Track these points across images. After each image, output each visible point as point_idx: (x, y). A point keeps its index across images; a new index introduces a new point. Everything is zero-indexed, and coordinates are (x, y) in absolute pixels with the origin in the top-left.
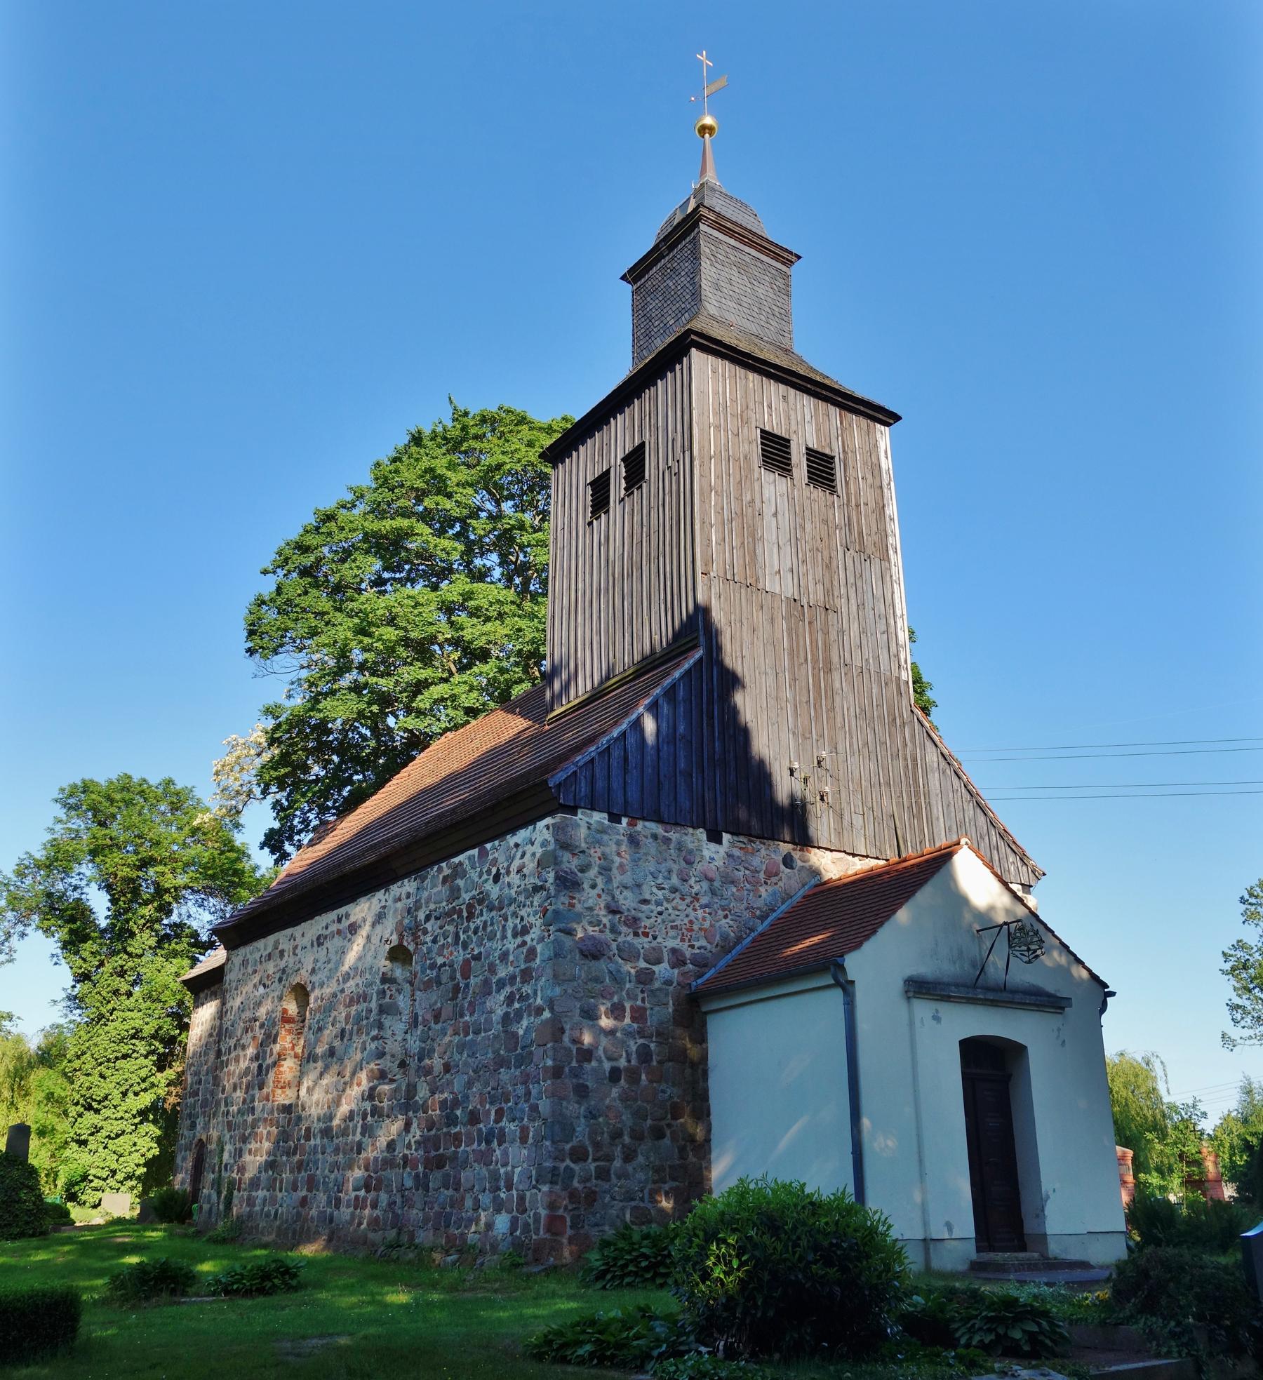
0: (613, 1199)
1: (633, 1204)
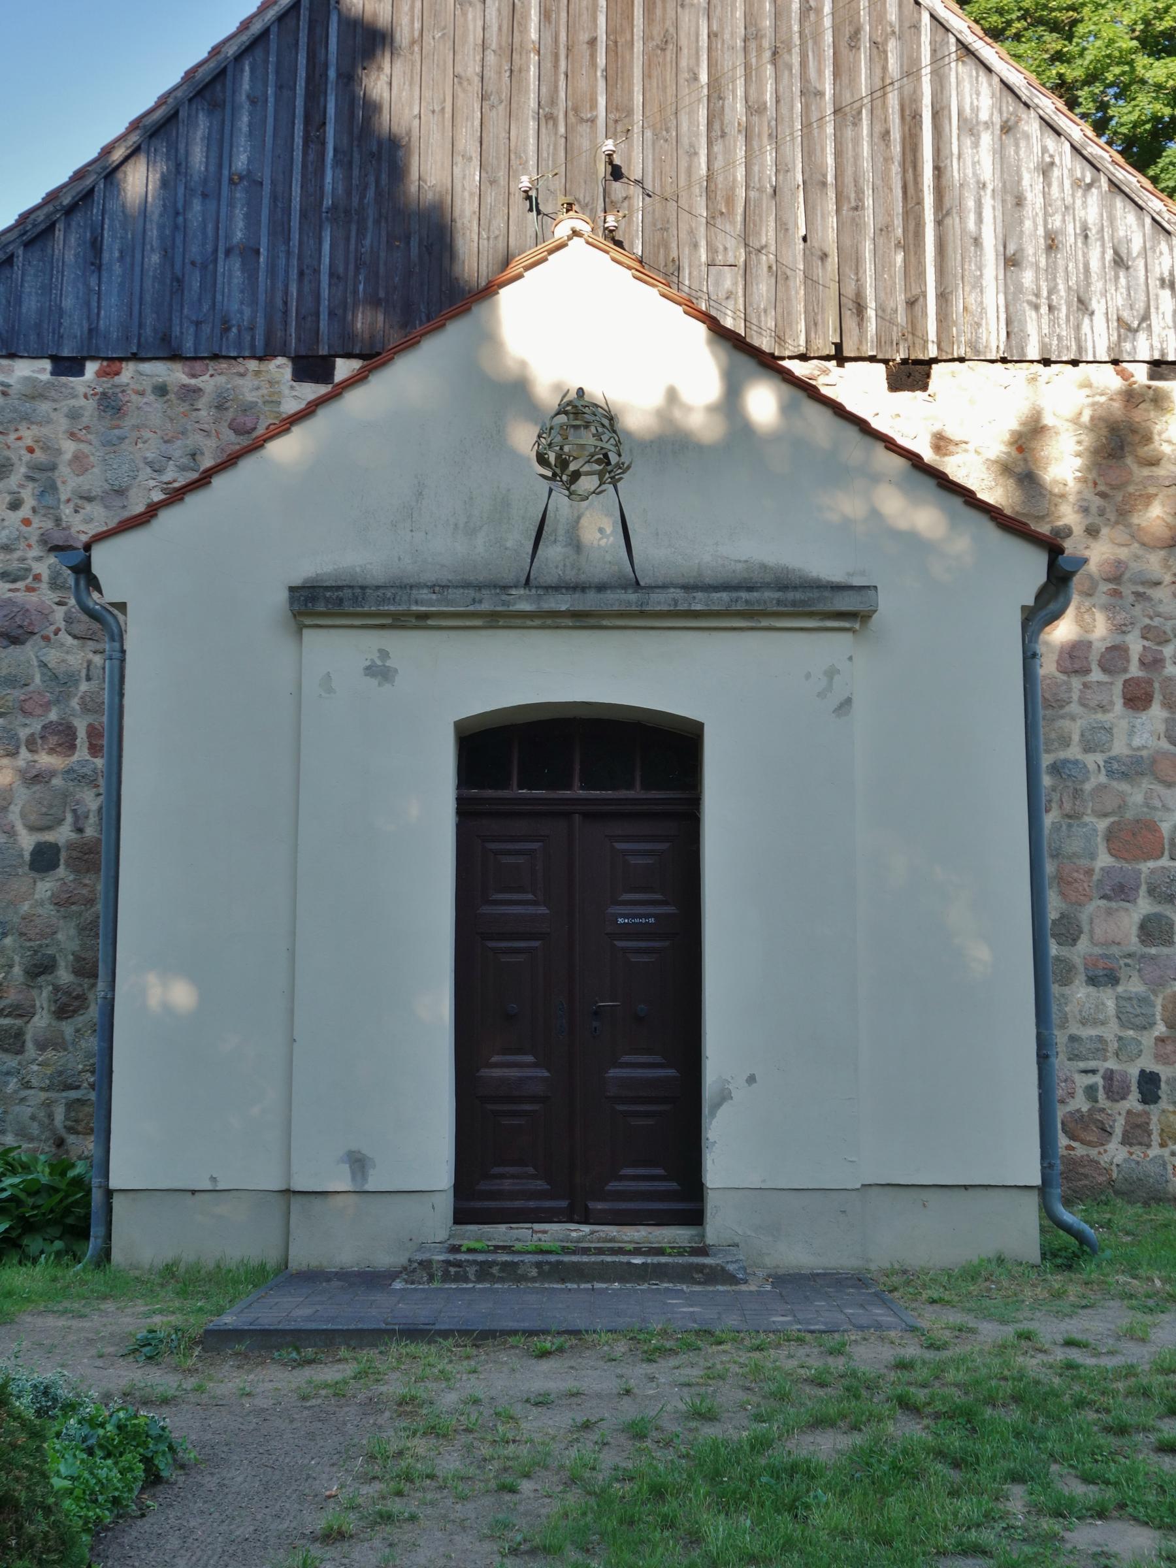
0: (27, 1086)
1: (73, 1094)
